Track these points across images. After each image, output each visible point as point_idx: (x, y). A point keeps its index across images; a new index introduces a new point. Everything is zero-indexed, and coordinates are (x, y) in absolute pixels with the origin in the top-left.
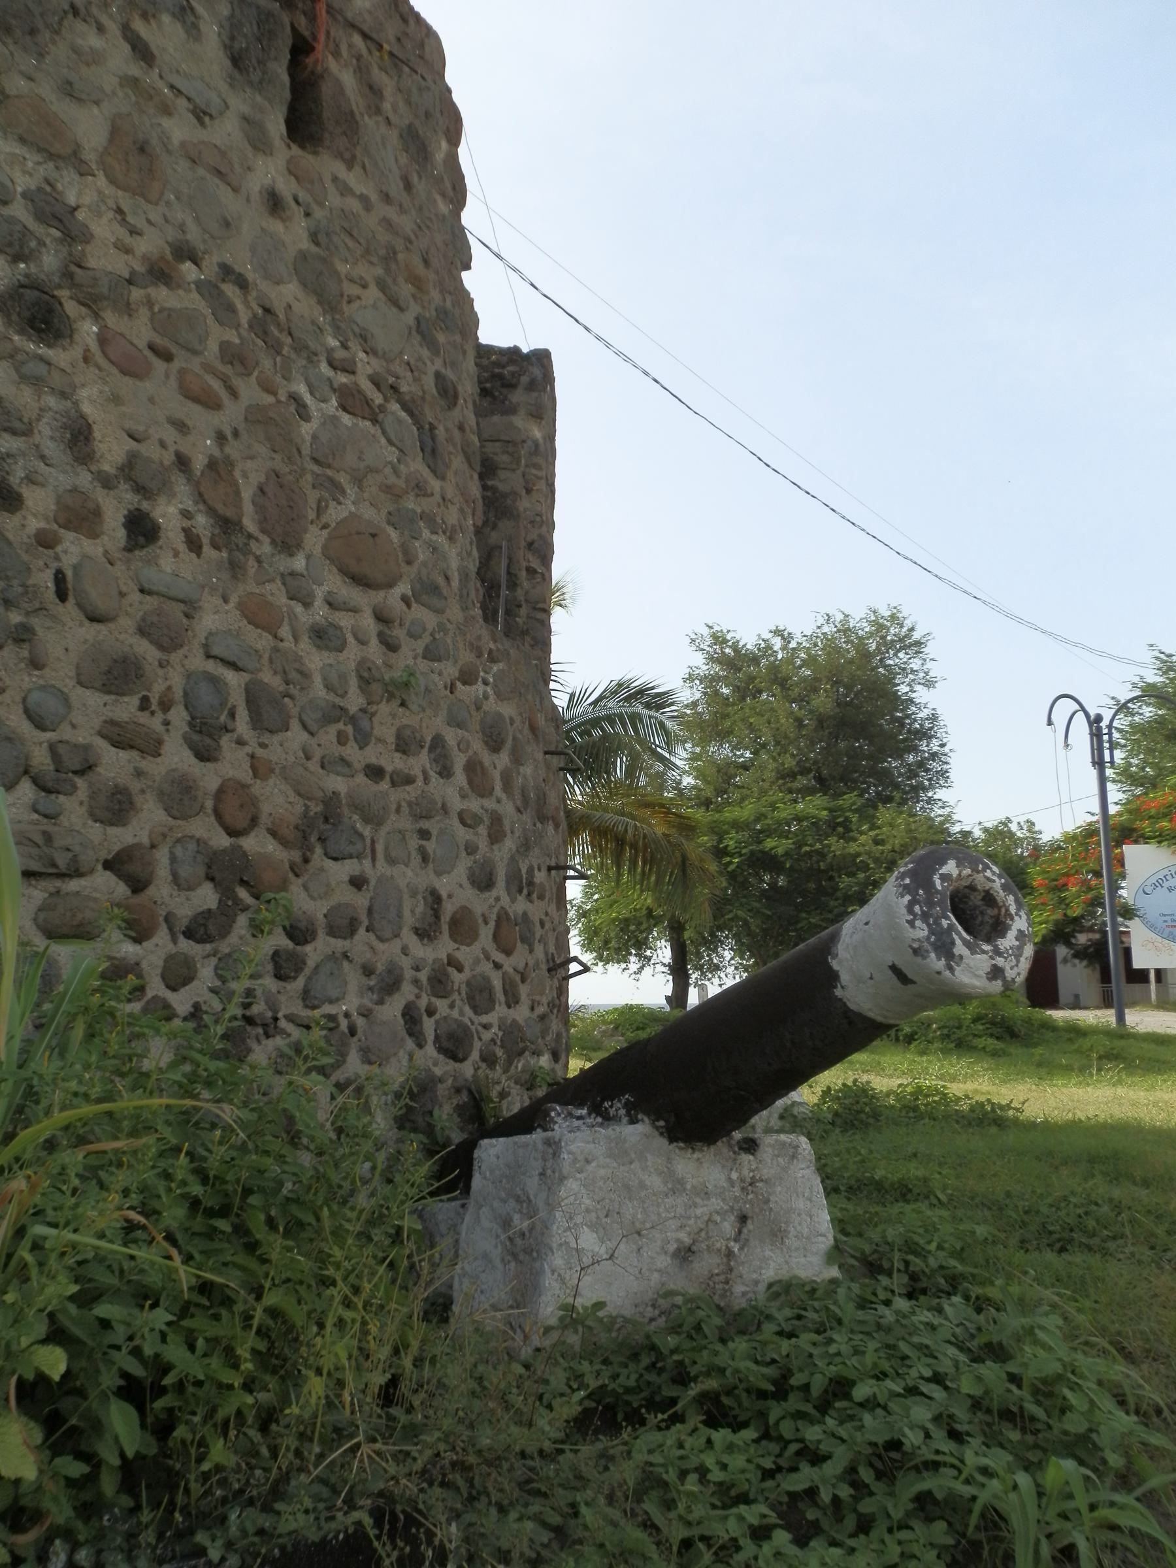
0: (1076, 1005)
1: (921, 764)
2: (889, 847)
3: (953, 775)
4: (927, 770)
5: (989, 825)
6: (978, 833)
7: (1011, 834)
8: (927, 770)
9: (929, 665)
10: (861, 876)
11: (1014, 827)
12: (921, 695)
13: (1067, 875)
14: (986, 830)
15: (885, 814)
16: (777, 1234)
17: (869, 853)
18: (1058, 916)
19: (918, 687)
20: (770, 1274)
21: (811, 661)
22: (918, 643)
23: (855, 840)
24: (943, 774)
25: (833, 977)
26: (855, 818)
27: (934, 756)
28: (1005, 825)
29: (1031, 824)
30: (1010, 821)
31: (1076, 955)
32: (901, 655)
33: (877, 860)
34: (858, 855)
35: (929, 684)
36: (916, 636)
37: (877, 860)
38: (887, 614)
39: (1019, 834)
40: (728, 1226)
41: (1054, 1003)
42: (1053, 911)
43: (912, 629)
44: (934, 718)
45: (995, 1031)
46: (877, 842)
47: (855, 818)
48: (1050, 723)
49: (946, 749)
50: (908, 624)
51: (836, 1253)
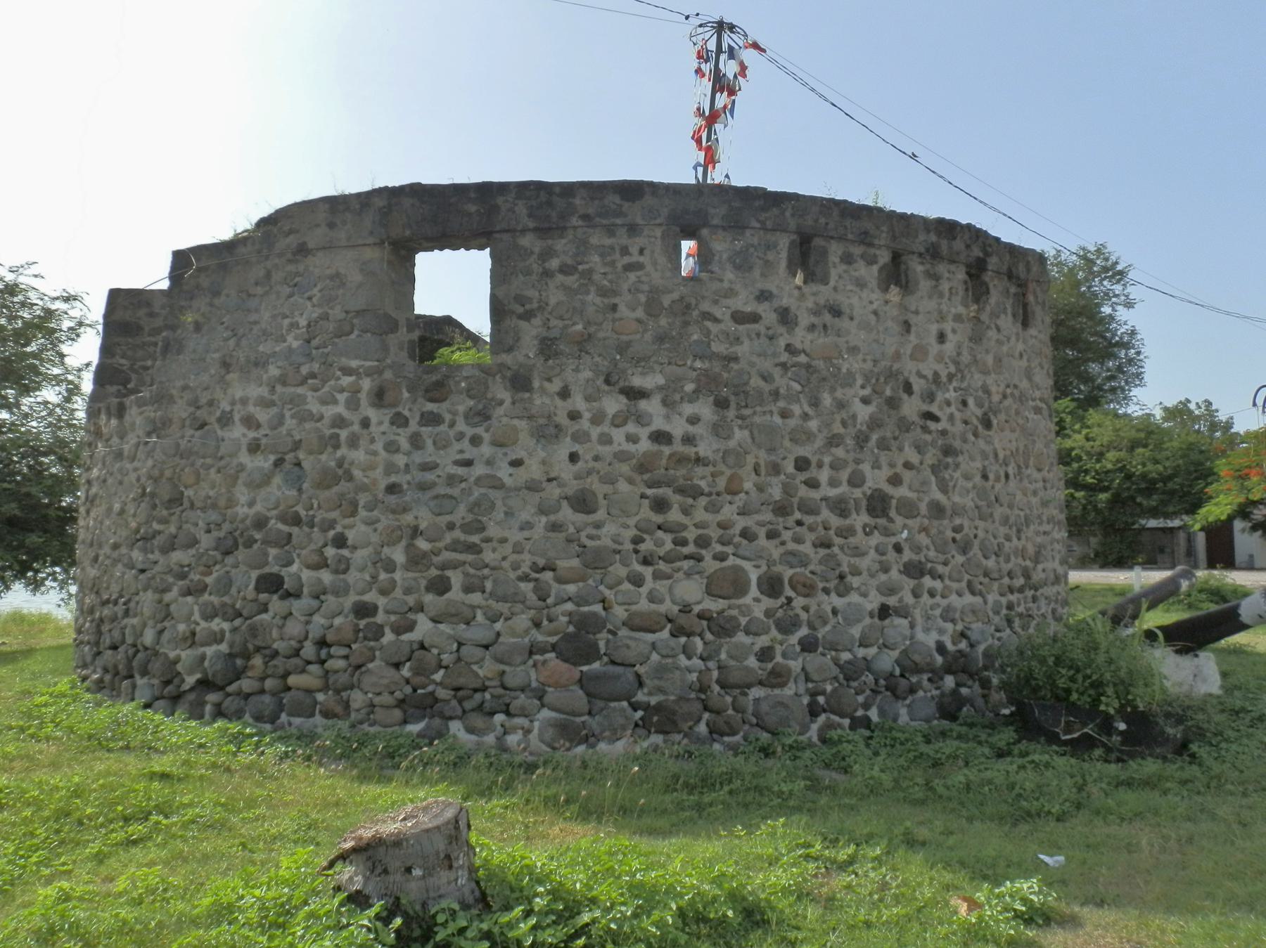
0: (1250, 567)
1: (1120, 369)
2: (1098, 443)
3: (1146, 377)
4: (1123, 373)
5: (1169, 405)
6: (1158, 414)
7: (1190, 412)
8: (1123, 373)
9: (1129, 289)
10: (1075, 465)
11: (1192, 406)
12: (1122, 313)
13: (1249, 467)
14: (1166, 409)
15: (1093, 416)
16: (1204, 681)
17: (1082, 448)
18: (1241, 499)
19: (1119, 308)
20: (1202, 692)
21: (716, 833)
22: (1121, 273)
23: (1069, 437)
24: (1139, 376)
25: (1239, 615)
26: (1068, 419)
27: (1130, 361)
28: (1185, 405)
29: (1209, 403)
30: (1188, 401)
31: (1254, 528)
32: (1105, 283)
33: (1088, 453)
34: (1073, 449)
35: (1129, 305)
36: (1119, 268)
37: (1088, 453)
38: (1093, 249)
39: (1197, 412)
40: (1191, 678)
41: (1230, 564)
42: (1237, 496)
43: (1117, 263)
44: (1133, 333)
45: (1216, 598)
46: (1088, 439)
47: (1068, 419)
48: (1255, 404)
49: (1142, 357)
50: (1113, 258)
51: (1222, 687)
